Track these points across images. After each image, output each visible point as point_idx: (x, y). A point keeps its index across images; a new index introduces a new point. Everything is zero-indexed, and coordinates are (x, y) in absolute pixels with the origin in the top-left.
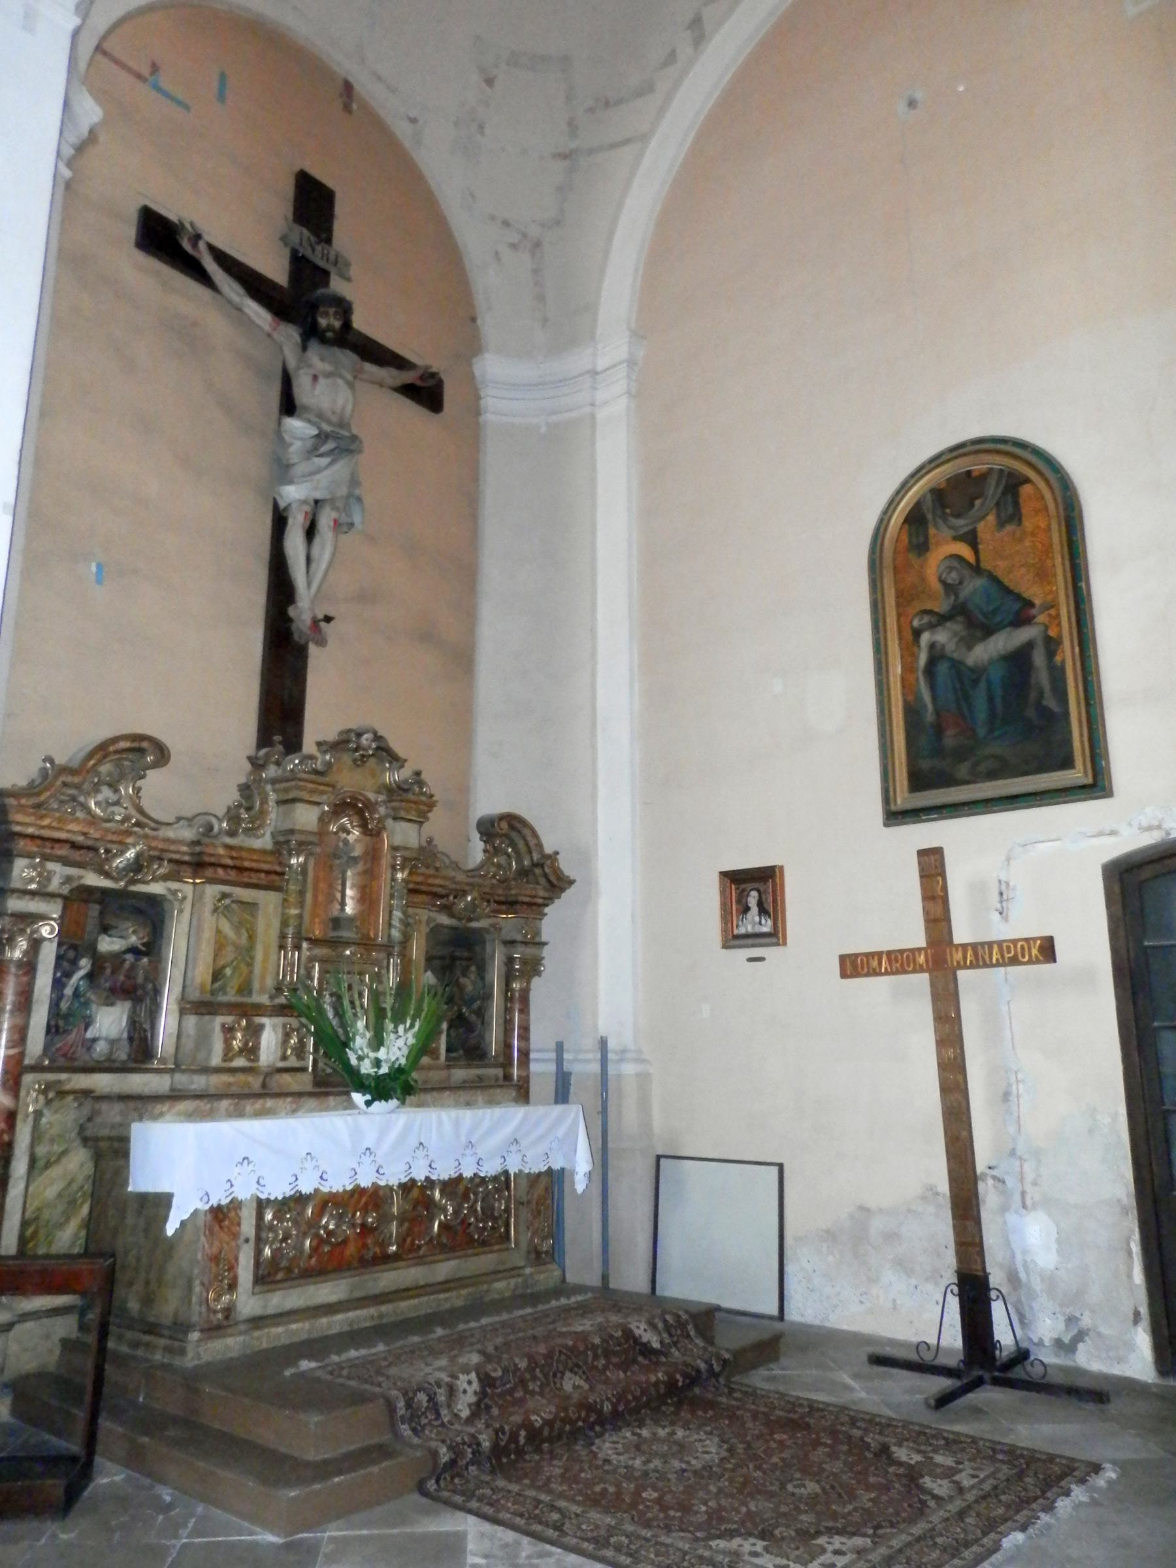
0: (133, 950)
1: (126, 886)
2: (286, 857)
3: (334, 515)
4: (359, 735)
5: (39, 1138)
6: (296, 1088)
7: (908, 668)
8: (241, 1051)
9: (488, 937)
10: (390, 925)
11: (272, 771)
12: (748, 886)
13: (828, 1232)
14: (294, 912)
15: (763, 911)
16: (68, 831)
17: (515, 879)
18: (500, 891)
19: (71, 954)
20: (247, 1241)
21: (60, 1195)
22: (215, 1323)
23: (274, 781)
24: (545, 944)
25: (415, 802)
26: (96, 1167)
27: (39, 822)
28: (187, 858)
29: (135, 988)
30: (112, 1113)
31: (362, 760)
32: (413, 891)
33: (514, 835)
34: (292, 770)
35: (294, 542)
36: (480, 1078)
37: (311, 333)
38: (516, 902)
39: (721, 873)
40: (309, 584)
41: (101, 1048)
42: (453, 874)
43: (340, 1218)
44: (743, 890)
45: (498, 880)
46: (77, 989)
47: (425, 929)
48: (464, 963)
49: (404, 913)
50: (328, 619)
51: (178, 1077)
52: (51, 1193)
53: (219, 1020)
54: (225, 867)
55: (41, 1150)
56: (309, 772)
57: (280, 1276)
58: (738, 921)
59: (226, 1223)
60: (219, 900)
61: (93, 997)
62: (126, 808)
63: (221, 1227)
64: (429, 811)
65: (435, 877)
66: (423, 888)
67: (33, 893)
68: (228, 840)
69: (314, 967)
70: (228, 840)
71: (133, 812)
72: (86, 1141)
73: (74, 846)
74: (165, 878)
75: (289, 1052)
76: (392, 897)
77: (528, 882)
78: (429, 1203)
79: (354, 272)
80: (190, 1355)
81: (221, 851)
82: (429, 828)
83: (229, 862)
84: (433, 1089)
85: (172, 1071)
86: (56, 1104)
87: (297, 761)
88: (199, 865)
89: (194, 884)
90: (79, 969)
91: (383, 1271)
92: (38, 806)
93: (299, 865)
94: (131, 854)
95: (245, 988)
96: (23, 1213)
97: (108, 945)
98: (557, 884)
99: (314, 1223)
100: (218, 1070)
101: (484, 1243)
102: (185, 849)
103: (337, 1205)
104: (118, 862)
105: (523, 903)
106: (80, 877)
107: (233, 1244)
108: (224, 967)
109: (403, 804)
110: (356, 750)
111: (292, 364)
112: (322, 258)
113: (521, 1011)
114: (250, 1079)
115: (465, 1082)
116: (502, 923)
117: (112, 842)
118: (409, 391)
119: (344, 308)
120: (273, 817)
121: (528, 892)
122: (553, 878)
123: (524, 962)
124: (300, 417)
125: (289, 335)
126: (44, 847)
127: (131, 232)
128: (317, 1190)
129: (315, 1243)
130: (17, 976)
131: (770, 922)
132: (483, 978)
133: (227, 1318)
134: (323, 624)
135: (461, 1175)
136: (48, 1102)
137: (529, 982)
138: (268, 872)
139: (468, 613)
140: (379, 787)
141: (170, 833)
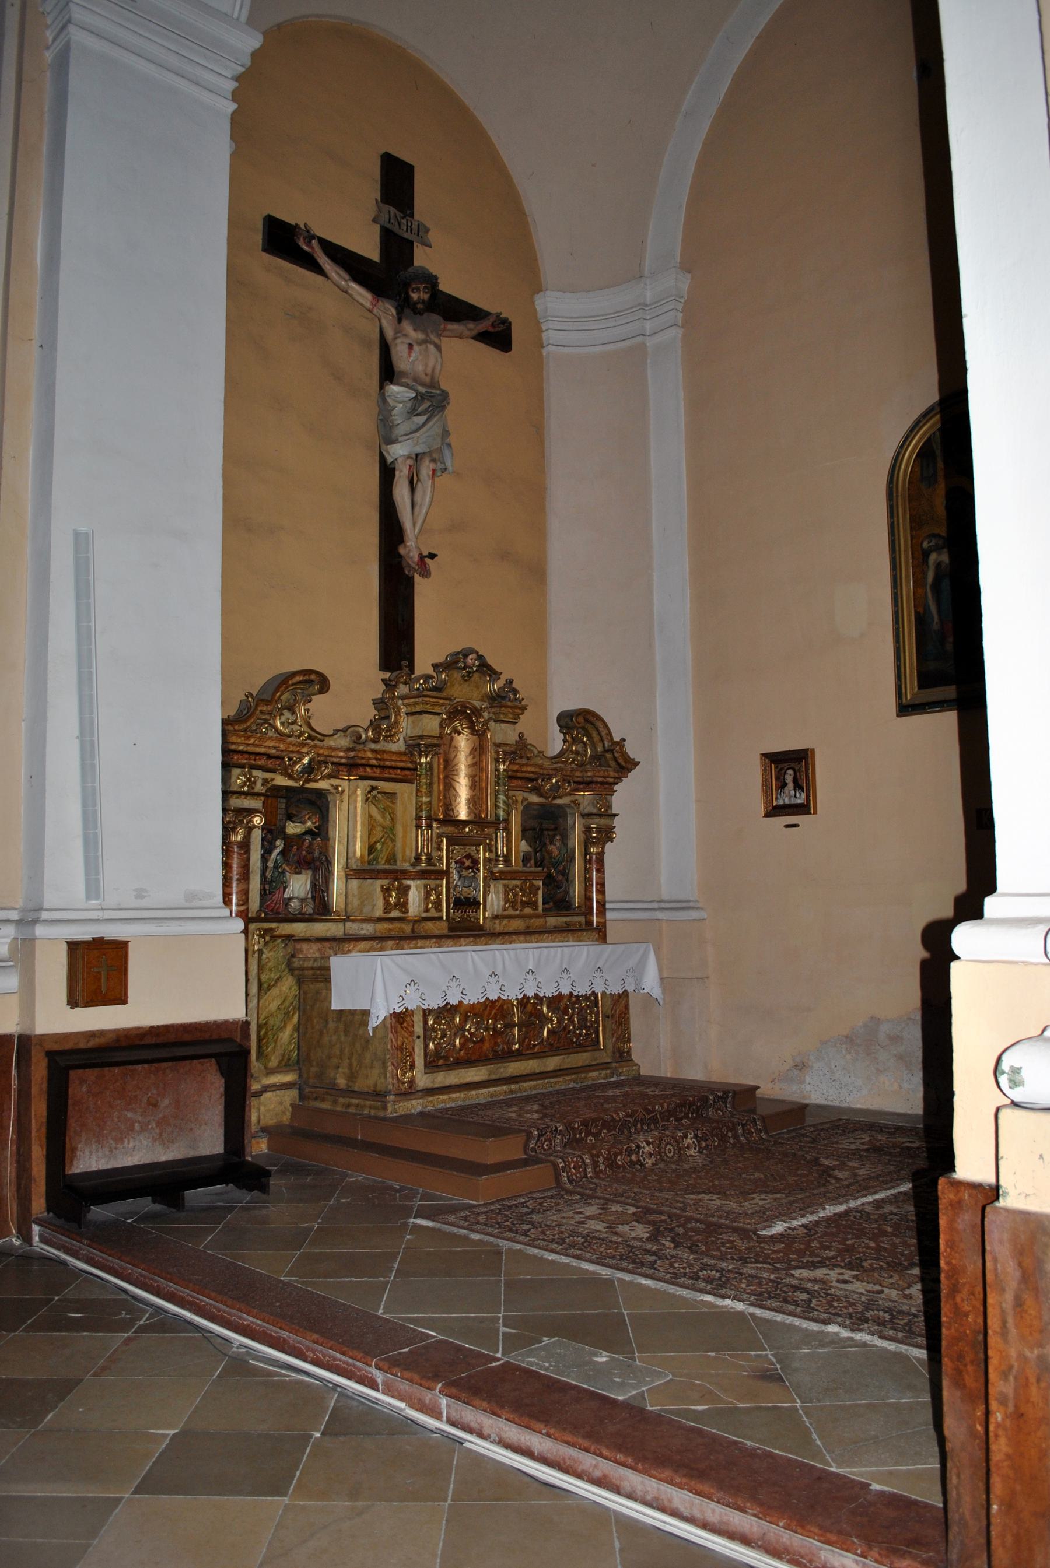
0: (309, 832)
1: (303, 784)
2: (417, 757)
3: (432, 466)
4: (466, 656)
5: (263, 967)
6: (437, 932)
7: (919, 582)
8: (396, 905)
9: (569, 811)
10: (497, 807)
11: (403, 689)
12: (786, 766)
13: (847, 1037)
14: (425, 799)
15: (797, 786)
16: (265, 747)
17: (590, 763)
18: (578, 774)
19: (269, 836)
20: (419, 1037)
21: (279, 1008)
22: (404, 1090)
23: (403, 698)
24: (616, 815)
25: (511, 707)
26: (299, 989)
27: (247, 742)
28: (343, 761)
29: (314, 860)
30: (311, 951)
31: (468, 676)
32: (511, 778)
33: (589, 727)
34: (418, 689)
35: (401, 492)
36: (568, 924)
37: (405, 308)
38: (591, 782)
39: (763, 755)
40: (414, 525)
41: (294, 904)
42: (541, 762)
43: (478, 1026)
44: (781, 769)
45: (577, 765)
46: (276, 861)
47: (520, 808)
48: (551, 833)
49: (507, 796)
50: (432, 556)
51: (348, 925)
52: (274, 1006)
53: (379, 883)
54: (372, 766)
55: (264, 977)
56: (430, 690)
57: (441, 1062)
58: (777, 794)
59: (405, 1024)
60: (369, 792)
61: (287, 868)
62: (301, 726)
63: (402, 1027)
64: (522, 714)
65: (527, 765)
66: (519, 775)
67: (246, 794)
68: (373, 746)
69: (442, 841)
70: (373, 746)
71: (305, 728)
72: (291, 970)
73: (269, 757)
74: (330, 776)
75: (430, 906)
76: (497, 784)
77: (600, 765)
78: (540, 1015)
79: (432, 236)
80: (390, 1109)
81: (369, 755)
82: (520, 727)
83: (375, 762)
84: (534, 933)
85: (344, 921)
86: (271, 945)
87: (421, 682)
88: (352, 767)
89: (349, 780)
90: (275, 847)
91: (513, 1061)
92: (245, 730)
93: (427, 763)
94: (306, 761)
95: (392, 859)
96: (258, 1018)
97: (293, 829)
98: (625, 766)
99: (461, 1028)
100: (380, 920)
101: (580, 1045)
102: (342, 754)
103: (475, 1015)
104: (298, 767)
105: (597, 782)
106: (272, 780)
107: (411, 1039)
108: (376, 843)
109: (503, 709)
110: (464, 668)
111: (389, 334)
112: (407, 231)
113: (598, 871)
114: (403, 926)
115: (555, 927)
116: (580, 800)
117: (292, 752)
118: (483, 337)
119: (431, 281)
120: (407, 727)
121: (601, 774)
122: (621, 761)
123: (599, 830)
124: (398, 384)
125: (387, 311)
126: (250, 759)
127: (258, 238)
128: (461, 1002)
129: (462, 1041)
130: (239, 854)
131: (803, 795)
132: (566, 845)
133: (410, 1087)
134: (427, 560)
135: (560, 993)
136: (266, 943)
137: (603, 848)
138: (402, 769)
139: (539, 531)
140: (482, 697)
141: (331, 743)
